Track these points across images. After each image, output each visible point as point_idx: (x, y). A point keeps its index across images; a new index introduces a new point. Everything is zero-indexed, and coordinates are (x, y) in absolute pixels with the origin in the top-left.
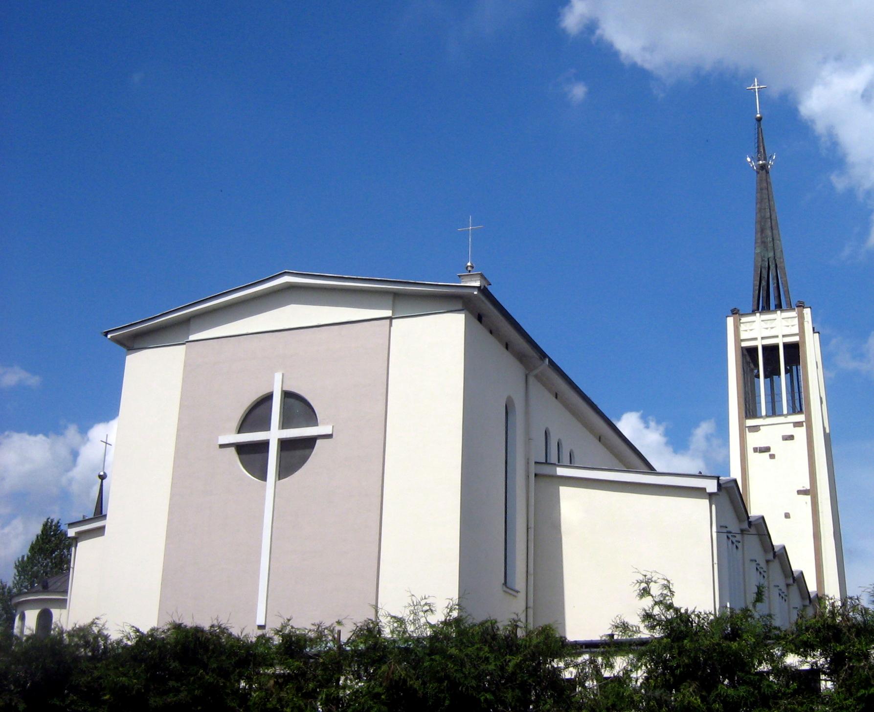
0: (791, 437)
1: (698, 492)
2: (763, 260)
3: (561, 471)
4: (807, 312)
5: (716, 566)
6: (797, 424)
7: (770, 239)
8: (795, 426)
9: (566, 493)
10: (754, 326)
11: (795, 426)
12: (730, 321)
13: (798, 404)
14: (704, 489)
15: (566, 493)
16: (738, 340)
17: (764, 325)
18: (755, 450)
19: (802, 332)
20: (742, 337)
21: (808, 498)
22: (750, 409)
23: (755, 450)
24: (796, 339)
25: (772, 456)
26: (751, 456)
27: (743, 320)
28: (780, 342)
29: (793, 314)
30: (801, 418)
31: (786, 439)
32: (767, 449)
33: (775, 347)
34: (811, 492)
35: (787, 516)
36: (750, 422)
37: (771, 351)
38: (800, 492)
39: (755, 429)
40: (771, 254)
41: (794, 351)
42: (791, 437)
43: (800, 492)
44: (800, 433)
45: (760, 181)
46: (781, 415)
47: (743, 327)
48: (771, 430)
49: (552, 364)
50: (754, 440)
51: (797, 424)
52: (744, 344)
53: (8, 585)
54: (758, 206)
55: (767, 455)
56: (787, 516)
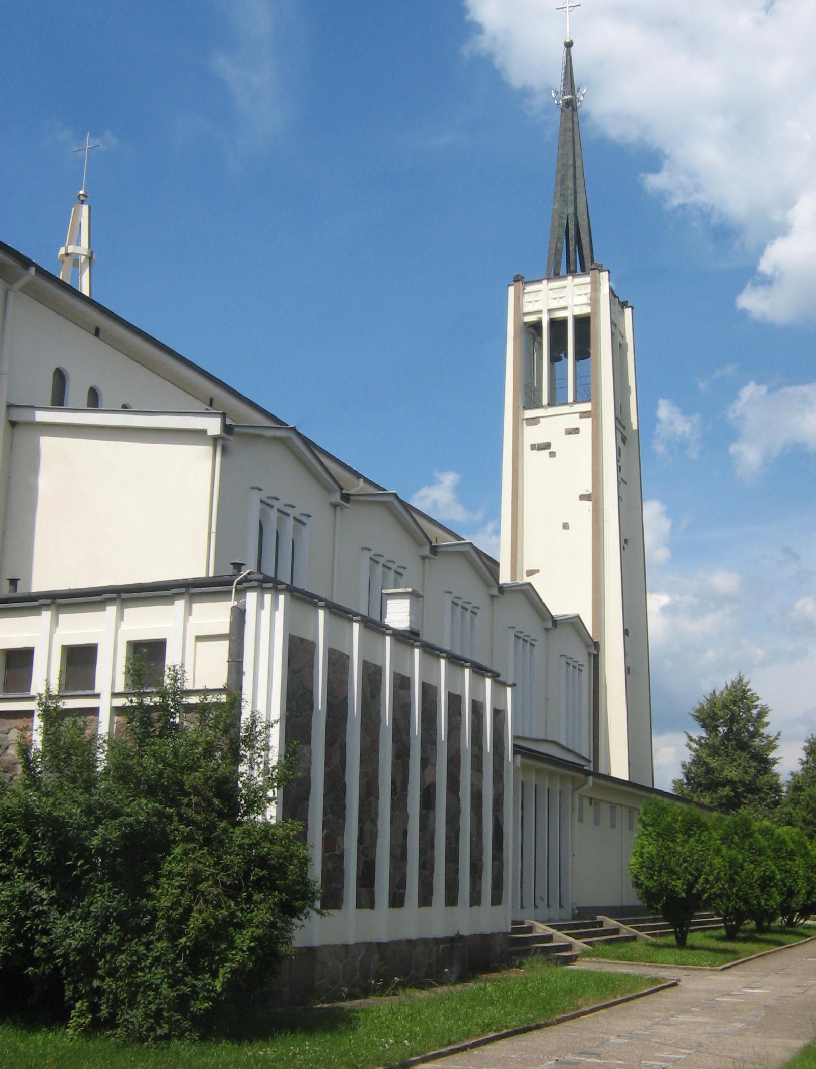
0: (576, 431)
1: (197, 435)
2: (560, 217)
3: (41, 416)
4: (604, 275)
5: (213, 536)
6: (583, 415)
7: (571, 191)
8: (581, 417)
9: (48, 444)
10: (540, 296)
11: (581, 417)
12: (511, 290)
13: (586, 391)
14: (204, 432)
15: (48, 444)
16: (519, 313)
17: (552, 294)
18: (533, 447)
19: (594, 302)
20: (526, 310)
21: (589, 504)
22: (530, 398)
23: (533, 447)
24: (587, 310)
25: (552, 454)
26: (527, 451)
27: (528, 289)
28: (569, 314)
29: (587, 279)
30: (587, 407)
31: (570, 434)
32: (547, 446)
33: (564, 322)
34: (594, 497)
35: (566, 526)
36: (529, 414)
37: (558, 325)
38: (582, 497)
39: (534, 421)
40: (571, 210)
41: (584, 323)
42: (576, 431)
43: (582, 497)
44: (586, 425)
45: (564, 121)
46: (566, 403)
47: (526, 298)
48: (552, 423)
49: (40, 271)
50: (531, 435)
51: (583, 415)
52: (527, 319)
53: (776, 769)
54: (561, 152)
55: (546, 452)
56: (566, 526)
